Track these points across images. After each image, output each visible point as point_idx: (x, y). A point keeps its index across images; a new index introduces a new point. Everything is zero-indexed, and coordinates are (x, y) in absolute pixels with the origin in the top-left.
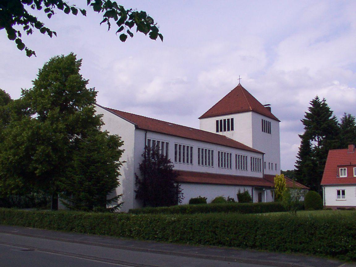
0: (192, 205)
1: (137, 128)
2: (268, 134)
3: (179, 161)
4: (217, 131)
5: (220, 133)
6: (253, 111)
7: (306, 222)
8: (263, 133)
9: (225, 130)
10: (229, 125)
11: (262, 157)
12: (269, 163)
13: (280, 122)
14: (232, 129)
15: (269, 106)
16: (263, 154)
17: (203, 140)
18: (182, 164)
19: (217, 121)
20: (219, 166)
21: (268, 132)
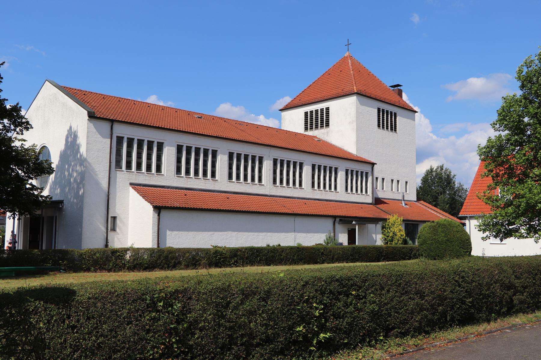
0: (350, 246)
1: (92, 116)
2: (391, 133)
3: (203, 174)
4: (306, 129)
5: (310, 133)
6: (358, 94)
7: (95, 254)
8: (381, 131)
9: (311, 128)
10: (319, 120)
11: (371, 170)
12: (392, 180)
13: (416, 114)
14: (328, 125)
15: (399, 88)
16: (373, 164)
17: (290, 147)
18: (256, 186)
19: (306, 113)
20: (313, 186)
21: (391, 129)
